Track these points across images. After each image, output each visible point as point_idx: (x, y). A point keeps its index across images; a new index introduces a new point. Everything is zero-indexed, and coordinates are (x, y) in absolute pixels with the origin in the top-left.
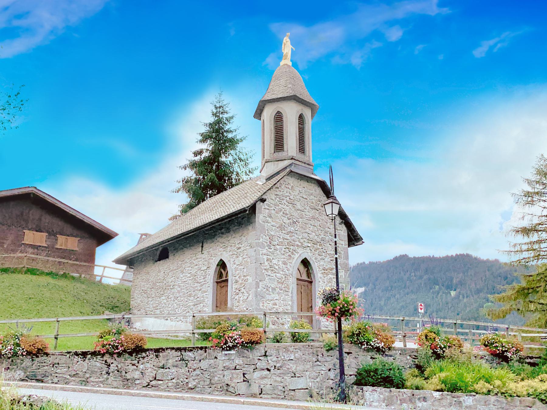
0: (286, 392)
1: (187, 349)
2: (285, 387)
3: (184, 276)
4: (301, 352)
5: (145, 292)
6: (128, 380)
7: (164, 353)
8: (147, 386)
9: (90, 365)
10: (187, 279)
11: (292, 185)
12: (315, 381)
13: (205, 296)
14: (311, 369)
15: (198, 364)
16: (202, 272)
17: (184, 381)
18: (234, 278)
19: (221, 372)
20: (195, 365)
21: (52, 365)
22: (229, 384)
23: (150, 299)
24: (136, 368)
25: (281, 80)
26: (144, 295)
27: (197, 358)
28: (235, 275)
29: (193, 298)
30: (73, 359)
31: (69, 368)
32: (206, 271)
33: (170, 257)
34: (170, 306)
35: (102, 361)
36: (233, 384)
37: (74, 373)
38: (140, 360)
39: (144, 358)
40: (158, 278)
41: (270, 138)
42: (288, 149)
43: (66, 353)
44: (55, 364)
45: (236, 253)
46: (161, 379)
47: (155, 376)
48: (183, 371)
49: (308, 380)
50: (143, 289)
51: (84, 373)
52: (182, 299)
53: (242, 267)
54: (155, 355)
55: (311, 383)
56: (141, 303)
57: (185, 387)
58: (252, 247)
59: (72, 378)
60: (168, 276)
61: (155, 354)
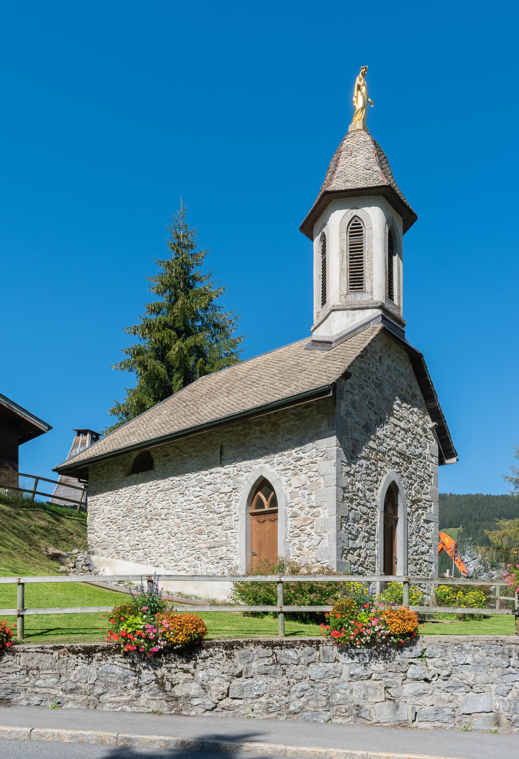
0: (458, 718)
1: (285, 643)
2: (455, 709)
3: (186, 501)
4: (483, 650)
5: (113, 521)
6: (177, 699)
7: (242, 651)
8: (213, 709)
9: (102, 672)
10: (193, 505)
11: (380, 354)
12: (505, 698)
13: (230, 535)
14: (499, 680)
15: (305, 671)
16: (223, 495)
17: (282, 700)
18: (290, 509)
19: (346, 685)
20: (300, 672)
21: (24, 672)
22: (361, 704)
23: (123, 533)
24: (192, 677)
25: (358, 158)
26: (112, 525)
27: (302, 660)
28: (290, 505)
29: (206, 536)
30: (68, 660)
31: (60, 676)
32: (231, 495)
33: (156, 468)
34: (162, 546)
35: (125, 663)
36: (368, 706)
37: (70, 686)
38: (198, 664)
39: (204, 659)
40: (137, 501)
41: (341, 265)
42: (372, 288)
43: (51, 648)
44: (32, 669)
45: (292, 467)
46: (239, 697)
47: (226, 691)
48: (279, 682)
49: (494, 698)
50: (109, 516)
51: (91, 686)
52: (185, 536)
53: (307, 492)
54: (226, 654)
55: (499, 702)
56: (106, 537)
57: (284, 710)
58: (329, 458)
59: (69, 696)
60: (155, 500)
61: (224, 652)
